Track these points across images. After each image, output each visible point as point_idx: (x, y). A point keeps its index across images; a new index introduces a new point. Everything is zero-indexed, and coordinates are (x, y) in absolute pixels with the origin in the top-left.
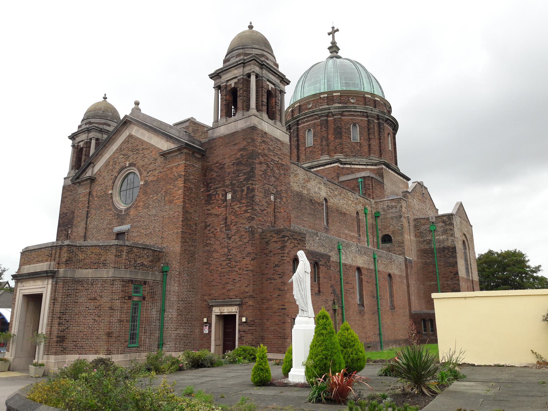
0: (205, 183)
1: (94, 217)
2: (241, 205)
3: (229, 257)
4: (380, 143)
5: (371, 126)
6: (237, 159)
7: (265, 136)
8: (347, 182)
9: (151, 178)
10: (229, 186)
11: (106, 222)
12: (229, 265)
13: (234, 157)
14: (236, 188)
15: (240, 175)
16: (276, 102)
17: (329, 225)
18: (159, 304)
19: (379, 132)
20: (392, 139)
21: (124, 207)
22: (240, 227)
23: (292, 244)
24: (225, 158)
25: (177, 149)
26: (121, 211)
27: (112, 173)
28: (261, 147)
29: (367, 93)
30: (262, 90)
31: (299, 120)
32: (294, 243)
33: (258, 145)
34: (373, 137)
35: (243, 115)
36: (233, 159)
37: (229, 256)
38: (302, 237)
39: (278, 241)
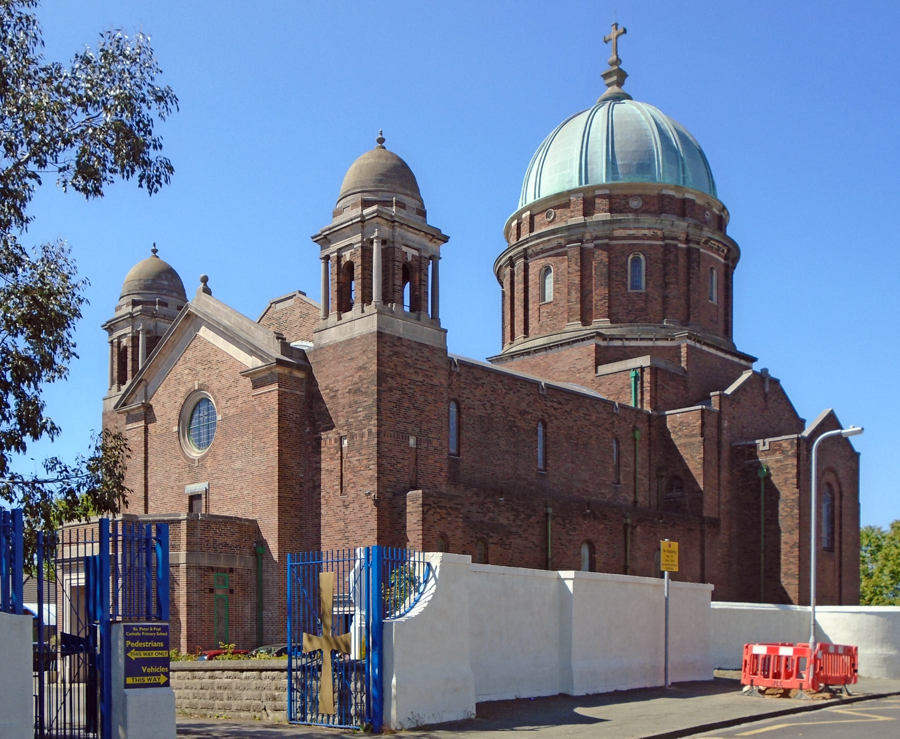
0: (312, 419)
1: (156, 468)
2: (361, 457)
3: (346, 534)
4: (688, 290)
5: (672, 257)
6: (354, 384)
7: (399, 344)
8: (611, 376)
9: (232, 411)
10: (344, 426)
11: (173, 477)
12: (347, 545)
13: (350, 380)
14: (353, 431)
15: (359, 410)
16: (420, 280)
17: (547, 468)
18: (254, 599)
19: (689, 268)
20: (722, 278)
21: (198, 453)
22: (360, 490)
23: (435, 515)
24: (338, 381)
25: (265, 367)
26: (193, 461)
27: (176, 399)
28: (390, 364)
29: (667, 187)
30: (394, 265)
31: (528, 248)
32: (439, 513)
33: (386, 361)
34: (672, 280)
35: (363, 311)
36: (348, 383)
37: (346, 532)
38: (455, 504)
39: (413, 512)
